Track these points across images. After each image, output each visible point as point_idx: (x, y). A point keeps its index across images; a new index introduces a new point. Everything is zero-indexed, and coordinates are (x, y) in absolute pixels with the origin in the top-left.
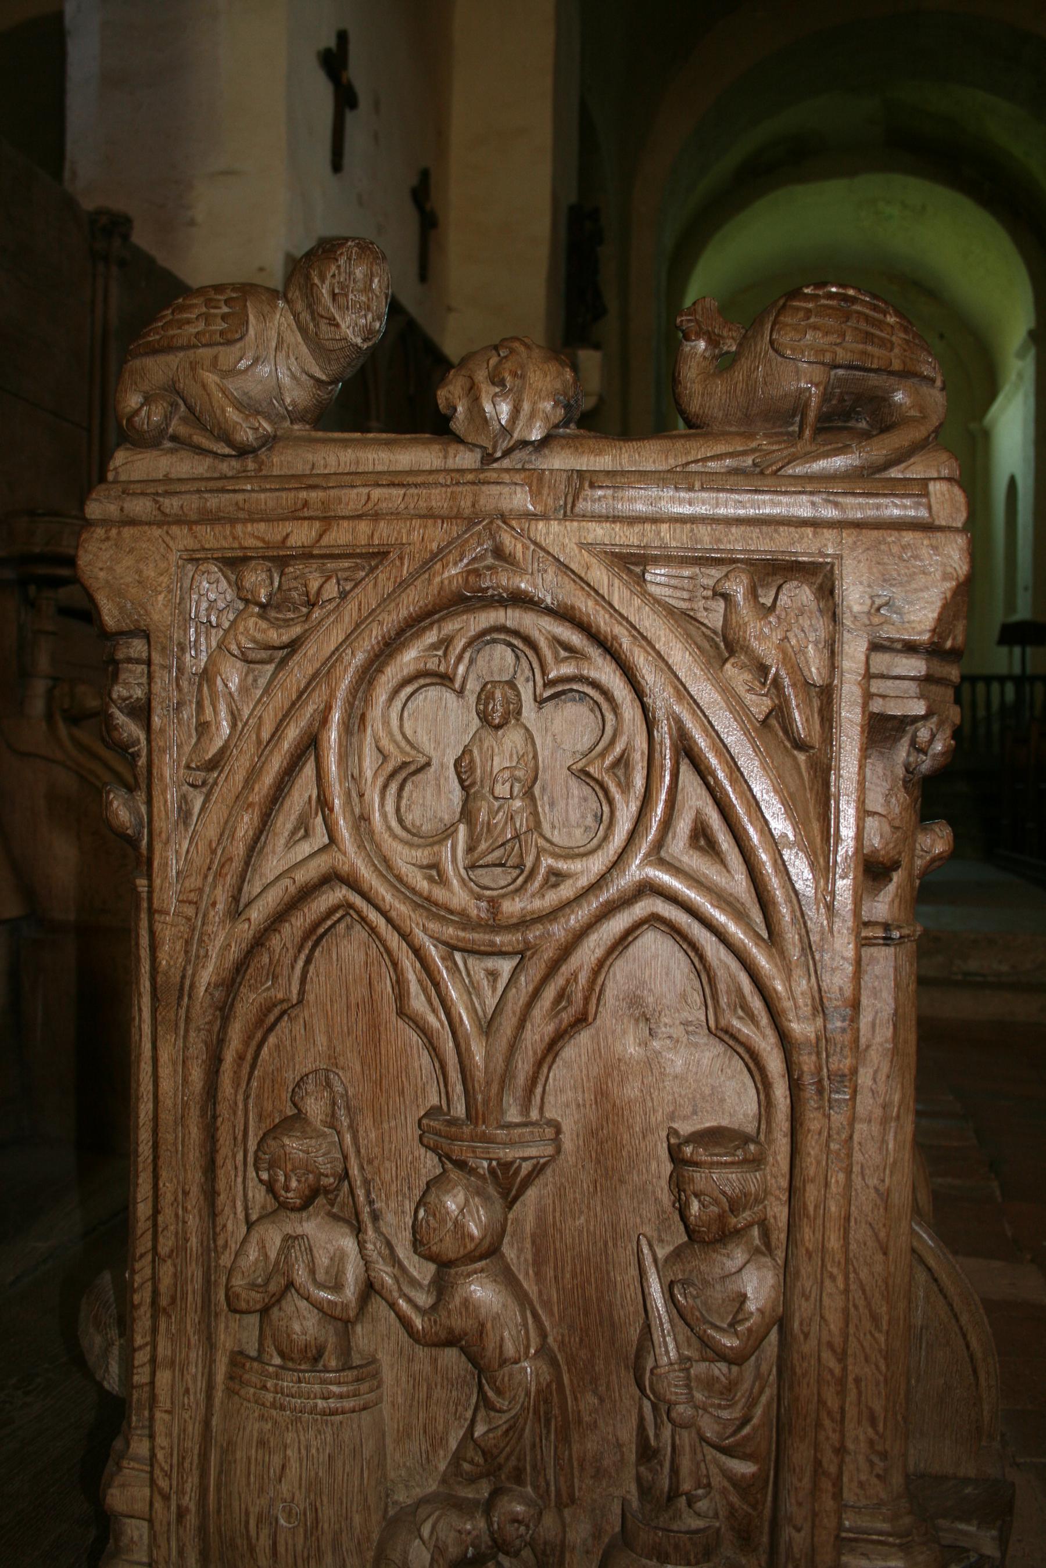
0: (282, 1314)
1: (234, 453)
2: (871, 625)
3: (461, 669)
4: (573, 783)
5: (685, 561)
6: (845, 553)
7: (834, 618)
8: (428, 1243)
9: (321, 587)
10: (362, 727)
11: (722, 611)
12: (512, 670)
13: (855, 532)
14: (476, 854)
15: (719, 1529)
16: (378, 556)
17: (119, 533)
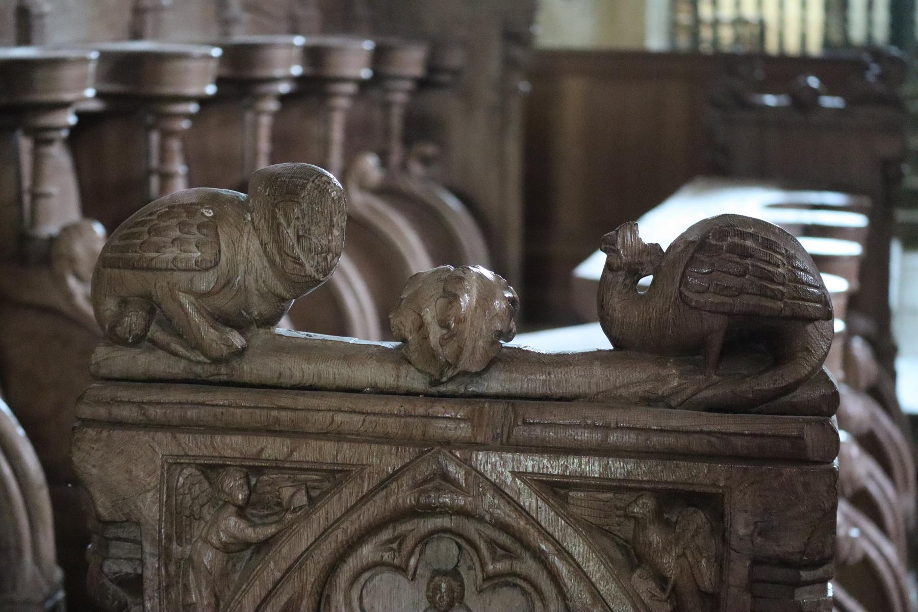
3: (413, 562)
9: (292, 496)
10: (327, 606)
12: (456, 559)
17: (109, 436)
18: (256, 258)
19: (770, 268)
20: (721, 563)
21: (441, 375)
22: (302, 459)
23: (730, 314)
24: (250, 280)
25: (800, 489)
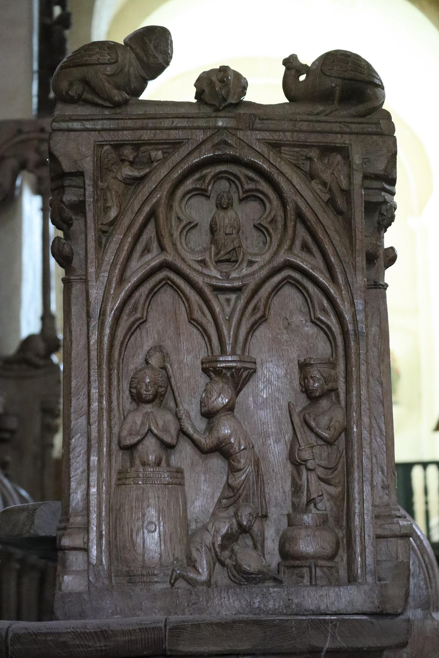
0: (144, 446)
2: (363, 168)
3: (210, 188)
4: (254, 230)
5: (294, 146)
6: (352, 143)
8: (208, 404)
11: (309, 165)
13: (355, 136)
14: (219, 256)
15: (327, 515)
16: (176, 144)
18: (134, 61)
19: (359, 62)
21: (220, 106)
22: (160, 138)
23: (344, 79)
24: (132, 70)
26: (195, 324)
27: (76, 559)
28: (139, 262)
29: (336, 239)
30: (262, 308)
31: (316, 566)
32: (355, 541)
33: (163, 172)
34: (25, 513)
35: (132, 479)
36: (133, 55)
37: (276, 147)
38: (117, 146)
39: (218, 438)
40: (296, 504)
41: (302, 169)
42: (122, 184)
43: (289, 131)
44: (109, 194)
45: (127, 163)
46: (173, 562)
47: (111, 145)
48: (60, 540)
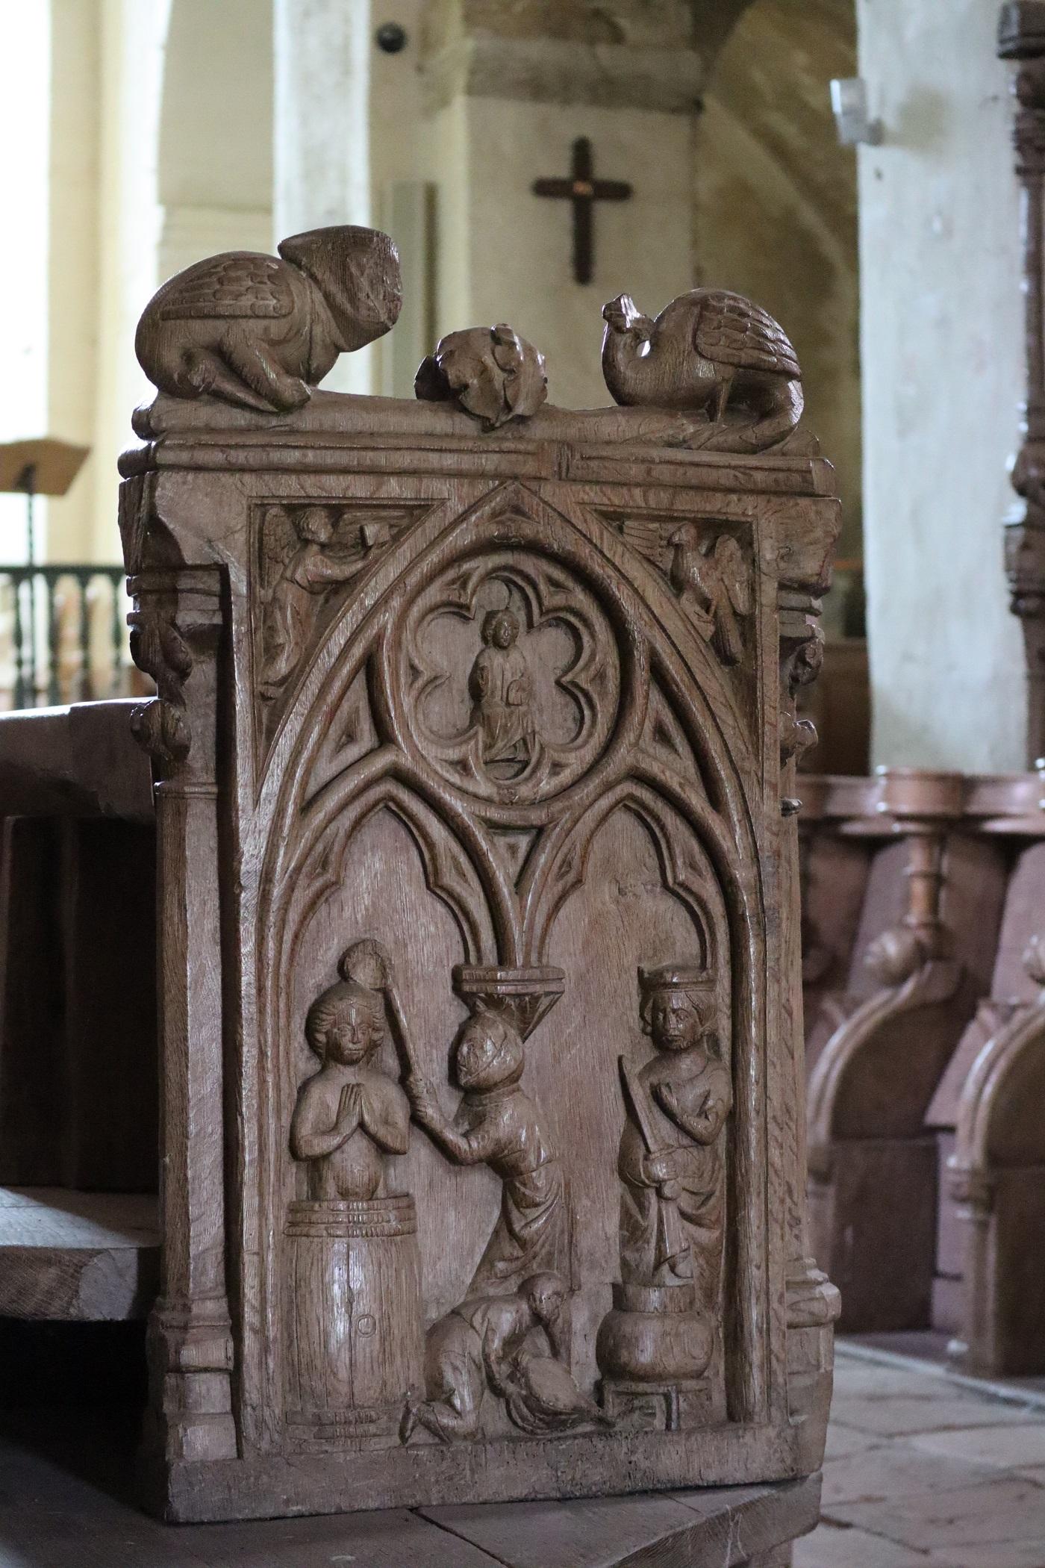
0: (345, 1155)
1: (275, 410)
7: (754, 563)
11: (672, 557)
14: (494, 751)
16: (418, 510)
20: (753, 589)
23: (738, 366)
24: (318, 330)
25: (812, 515)
26: (444, 895)
27: (208, 1390)
28: (333, 764)
29: (727, 720)
30: (576, 862)
31: (679, 1392)
32: (751, 1340)
33: (391, 571)
34: (53, 1271)
35: (323, 1226)
36: (318, 296)
37: (612, 519)
38: (294, 510)
39: (498, 1142)
40: (633, 1264)
41: (657, 566)
42: (306, 594)
43: (638, 485)
44: (278, 616)
45: (315, 548)
46: (405, 1394)
47: (283, 505)
48: (178, 1352)
